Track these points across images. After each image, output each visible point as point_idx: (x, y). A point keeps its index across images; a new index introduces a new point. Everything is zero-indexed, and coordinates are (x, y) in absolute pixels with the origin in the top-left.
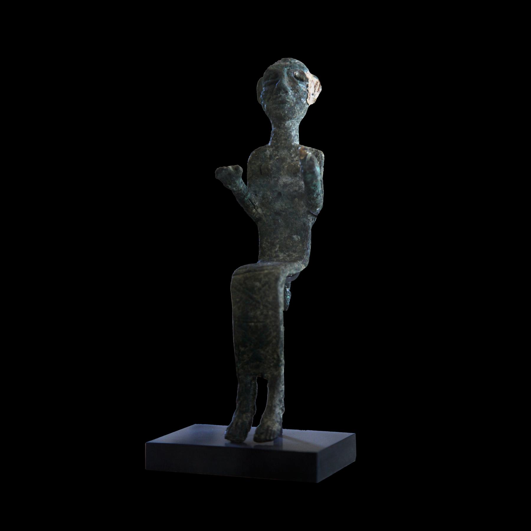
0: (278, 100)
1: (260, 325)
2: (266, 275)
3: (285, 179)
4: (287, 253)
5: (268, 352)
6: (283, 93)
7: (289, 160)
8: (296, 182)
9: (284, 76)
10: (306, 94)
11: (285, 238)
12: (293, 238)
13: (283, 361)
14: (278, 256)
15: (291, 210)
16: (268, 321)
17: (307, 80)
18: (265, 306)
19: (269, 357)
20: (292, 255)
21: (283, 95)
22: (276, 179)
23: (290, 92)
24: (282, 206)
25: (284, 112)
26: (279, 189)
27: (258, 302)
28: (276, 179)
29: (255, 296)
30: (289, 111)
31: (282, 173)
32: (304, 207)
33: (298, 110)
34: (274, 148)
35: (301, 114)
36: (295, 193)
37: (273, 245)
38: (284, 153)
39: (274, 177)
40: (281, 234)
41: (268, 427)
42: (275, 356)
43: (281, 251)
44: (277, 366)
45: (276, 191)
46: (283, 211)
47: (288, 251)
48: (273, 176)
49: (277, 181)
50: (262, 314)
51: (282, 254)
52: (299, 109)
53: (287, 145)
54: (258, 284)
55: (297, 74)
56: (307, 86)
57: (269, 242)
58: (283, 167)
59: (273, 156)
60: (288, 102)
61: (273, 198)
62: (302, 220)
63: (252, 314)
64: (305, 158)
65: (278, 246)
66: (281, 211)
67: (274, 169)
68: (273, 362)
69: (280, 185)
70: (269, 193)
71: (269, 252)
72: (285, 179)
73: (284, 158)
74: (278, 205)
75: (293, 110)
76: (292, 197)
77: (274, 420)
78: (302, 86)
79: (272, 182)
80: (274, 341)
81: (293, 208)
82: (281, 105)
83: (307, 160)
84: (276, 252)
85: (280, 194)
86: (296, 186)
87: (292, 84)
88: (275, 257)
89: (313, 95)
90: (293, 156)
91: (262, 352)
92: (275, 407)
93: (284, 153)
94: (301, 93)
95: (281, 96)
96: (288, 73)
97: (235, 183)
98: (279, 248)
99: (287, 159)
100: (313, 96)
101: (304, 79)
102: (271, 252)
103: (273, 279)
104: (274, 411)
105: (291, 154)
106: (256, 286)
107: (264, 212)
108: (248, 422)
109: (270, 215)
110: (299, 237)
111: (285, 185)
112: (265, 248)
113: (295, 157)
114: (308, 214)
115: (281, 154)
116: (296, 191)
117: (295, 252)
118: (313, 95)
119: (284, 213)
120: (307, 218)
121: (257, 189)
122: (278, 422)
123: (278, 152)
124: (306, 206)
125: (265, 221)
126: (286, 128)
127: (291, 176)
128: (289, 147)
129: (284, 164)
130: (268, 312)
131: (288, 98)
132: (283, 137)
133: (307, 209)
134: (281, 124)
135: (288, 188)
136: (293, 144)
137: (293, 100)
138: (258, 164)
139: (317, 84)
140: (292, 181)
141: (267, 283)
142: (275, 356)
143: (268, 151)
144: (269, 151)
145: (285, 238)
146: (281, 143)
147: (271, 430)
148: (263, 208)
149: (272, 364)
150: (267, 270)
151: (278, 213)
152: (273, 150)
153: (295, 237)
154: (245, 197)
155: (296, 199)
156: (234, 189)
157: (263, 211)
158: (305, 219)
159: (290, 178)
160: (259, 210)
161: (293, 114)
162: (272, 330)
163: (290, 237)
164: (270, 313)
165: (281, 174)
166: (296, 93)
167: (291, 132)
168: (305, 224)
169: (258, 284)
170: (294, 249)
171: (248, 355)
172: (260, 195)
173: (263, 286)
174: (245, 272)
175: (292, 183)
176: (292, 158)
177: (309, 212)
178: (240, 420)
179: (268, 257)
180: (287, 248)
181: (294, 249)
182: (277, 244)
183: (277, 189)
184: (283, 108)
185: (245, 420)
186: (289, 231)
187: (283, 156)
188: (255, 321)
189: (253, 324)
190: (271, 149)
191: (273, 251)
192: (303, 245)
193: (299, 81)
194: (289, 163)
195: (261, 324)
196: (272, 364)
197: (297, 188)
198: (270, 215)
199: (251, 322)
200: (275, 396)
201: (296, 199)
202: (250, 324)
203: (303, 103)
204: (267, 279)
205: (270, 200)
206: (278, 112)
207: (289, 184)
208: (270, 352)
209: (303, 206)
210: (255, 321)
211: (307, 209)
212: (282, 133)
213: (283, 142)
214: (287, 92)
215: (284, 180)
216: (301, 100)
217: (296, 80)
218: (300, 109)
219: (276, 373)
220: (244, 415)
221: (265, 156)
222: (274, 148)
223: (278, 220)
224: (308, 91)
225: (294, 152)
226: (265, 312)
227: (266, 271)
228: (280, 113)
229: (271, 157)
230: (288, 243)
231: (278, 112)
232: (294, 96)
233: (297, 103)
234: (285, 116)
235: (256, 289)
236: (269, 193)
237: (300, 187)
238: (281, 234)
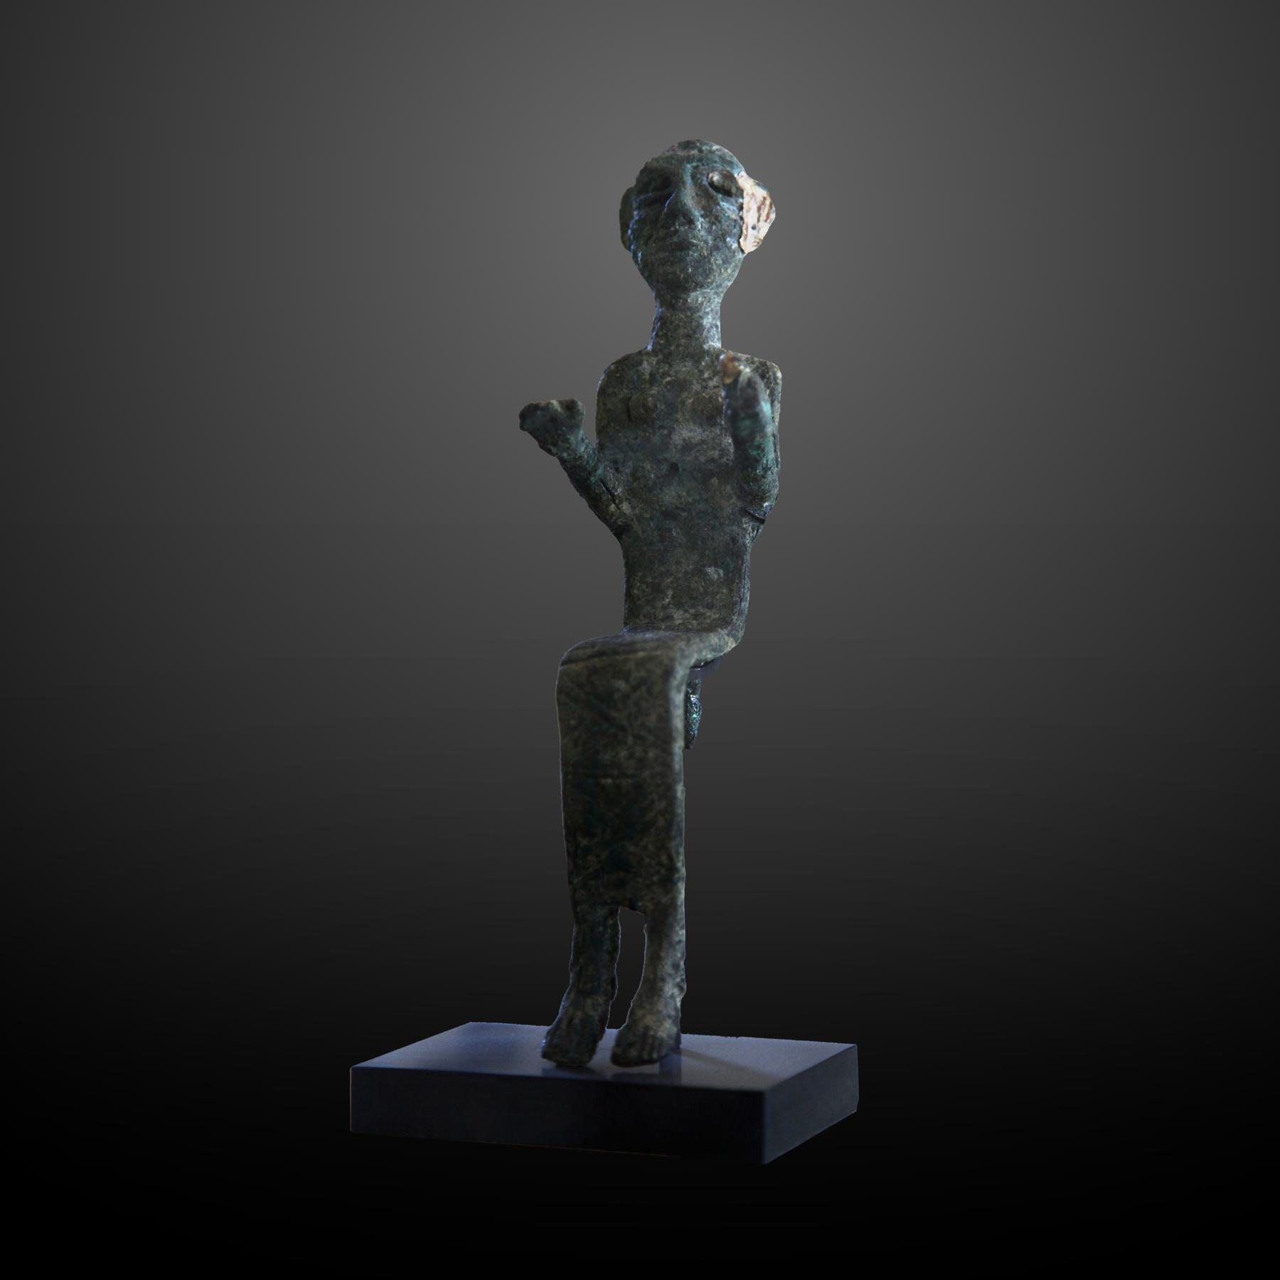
0: (669, 241)
1: (626, 783)
2: (641, 663)
3: (688, 432)
4: (692, 611)
5: (645, 848)
6: (683, 225)
7: (696, 387)
8: (713, 439)
9: (684, 183)
10: (738, 227)
11: (686, 573)
12: (706, 574)
13: (683, 871)
14: (670, 618)
15: (701, 506)
16: (646, 774)
17: (740, 192)
18: (638, 738)
19: (647, 860)
20: (703, 614)
21: (682, 229)
22: (665, 432)
23: (700, 223)
24: (679, 496)
25: (684, 270)
26: (673, 455)
27: (623, 729)
28: (665, 432)
29: (614, 714)
30: (695, 268)
31: (679, 416)
32: (734, 500)
33: (718, 266)
34: (660, 357)
35: (725, 275)
36: (711, 466)
37: (658, 590)
38: (684, 369)
39: (661, 427)
40: (678, 563)
41: (647, 1028)
42: (664, 859)
43: (679, 605)
44: (668, 882)
45: (666, 460)
46: (683, 510)
47: (693, 606)
48: (658, 423)
49: (669, 435)
50: (631, 756)
51: (681, 612)
52: (720, 262)
53: (691, 350)
54: (621, 685)
55: (716, 177)
56: (741, 208)
57: (647, 584)
58: (683, 403)
59: (658, 376)
60: (693, 245)
61: (657, 477)
62: (727, 529)
63: (607, 757)
64: (736, 381)
65: (670, 593)
66: (677, 508)
67: (661, 406)
68: (658, 872)
69: (676, 446)
70: (648, 466)
71: (648, 608)
72: (688, 432)
73: (685, 381)
74: (670, 495)
75: (707, 266)
76: (704, 475)
77: (660, 1012)
78: (728, 207)
79: (656, 439)
80: (661, 822)
81: (706, 500)
82: (678, 253)
83: (739, 386)
84: (665, 607)
85: (674, 467)
86: (714, 448)
87: (704, 202)
88: (662, 620)
89: (754, 228)
90: (706, 375)
91: (632, 848)
92: (663, 980)
93: (684, 369)
94: (725, 225)
95: (677, 231)
96: (693, 177)
97: (567, 441)
98: (673, 597)
99: (691, 384)
100: (755, 232)
101: (734, 190)
102: (654, 607)
103: (659, 672)
104: (661, 990)
105: (701, 372)
106: (618, 690)
107: (637, 511)
108: (597, 1018)
109: (651, 518)
110: (721, 572)
111: (688, 446)
112: (639, 599)
113: (710, 378)
114: (743, 516)
115: (677, 372)
116: (713, 460)
117: (710, 606)
118: (754, 228)
119: (684, 514)
120: (740, 527)
121: (620, 456)
122: (669, 1017)
123: (671, 366)
124: (739, 497)
125: (640, 532)
126: (689, 308)
127: (701, 425)
128: (698, 354)
129: (685, 394)
130: (646, 752)
131: (694, 237)
132: (681, 331)
133: (739, 504)
134: (677, 298)
135: (693, 454)
136: (706, 347)
137: (706, 242)
138: (621, 396)
139: (763, 203)
140: (704, 435)
141: (643, 682)
143: (645, 365)
144: (649, 363)
145: (686, 573)
146: (678, 346)
147: (654, 1037)
148: (634, 501)
149: (655, 879)
150: (643, 650)
151: (669, 514)
152: (658, 362)
153: (711, 570)
154: (590, 474)
155: (715, 481)
157: (633, 508)
158: (735, 528)
159: (700, 430)
160: (625, 507)
161: (707, 276)
162: (655, 796)
163: (700, 572)
164: (651, 754)
165: (677, 420)
166: (713, 223)
167: (701, 317)
168: (734, 540)
169: (621, 685)
170: (708, 599)
171: (598, 856)
172: (628, 471)
173: (635, 689)
174: (591, 657)
175: (703, 442)
176: (705, 380)
177: (745, 512)
178: (579, 1013)
179: (647, 621)
180: (691, 598)
181: (708, 599)
182: (669, 587)
183: (667, 455)
184: (682, 260)
185: (591, 1013)
186: (696, 557)
187: (681, 376)
188: (616, 773)
189: (609, 781)
190: (654, 360)
191: (659, 605)
192: (731, 591)
193: (720, 196)
194: (697, 393)
195: (630, 781)
196: (655, 879)
197: (716, 454)
198: (651, 518)
199: (606, 776)
200: (663, 954)
201: (715, 481)
202: (603, 781)
203: (729, 248)
204: (643, 673)
205: (651, 483)
206: (669, 269)
207: (697, 445)
208: (651, 847)
209: (730, 497)
210: (616, 773)
211: (739, 504)
212: (681, 320)
213: (683, 341)
214: (691, 222)
215: (685, 434)
216: (725, 240)
217: (714, 193)
218: (724, 262)
219: (664, 900)
220: (589, 1002)
221: (639, 377)
222: (660, 357)
223: (669, 530)
224: (742, 218)
225: (708, 366)
226: (639, 752)
227: (641, 654)
228: (675, 273)
229: (653, 380)
230: (693, 585)
231: (669, 269)
232: (709, 231)
233: (716, 248)
234: (686, 280)
235: (616, 696)
236: (648, 466)
237: (723, 452)
238: (678, 563)
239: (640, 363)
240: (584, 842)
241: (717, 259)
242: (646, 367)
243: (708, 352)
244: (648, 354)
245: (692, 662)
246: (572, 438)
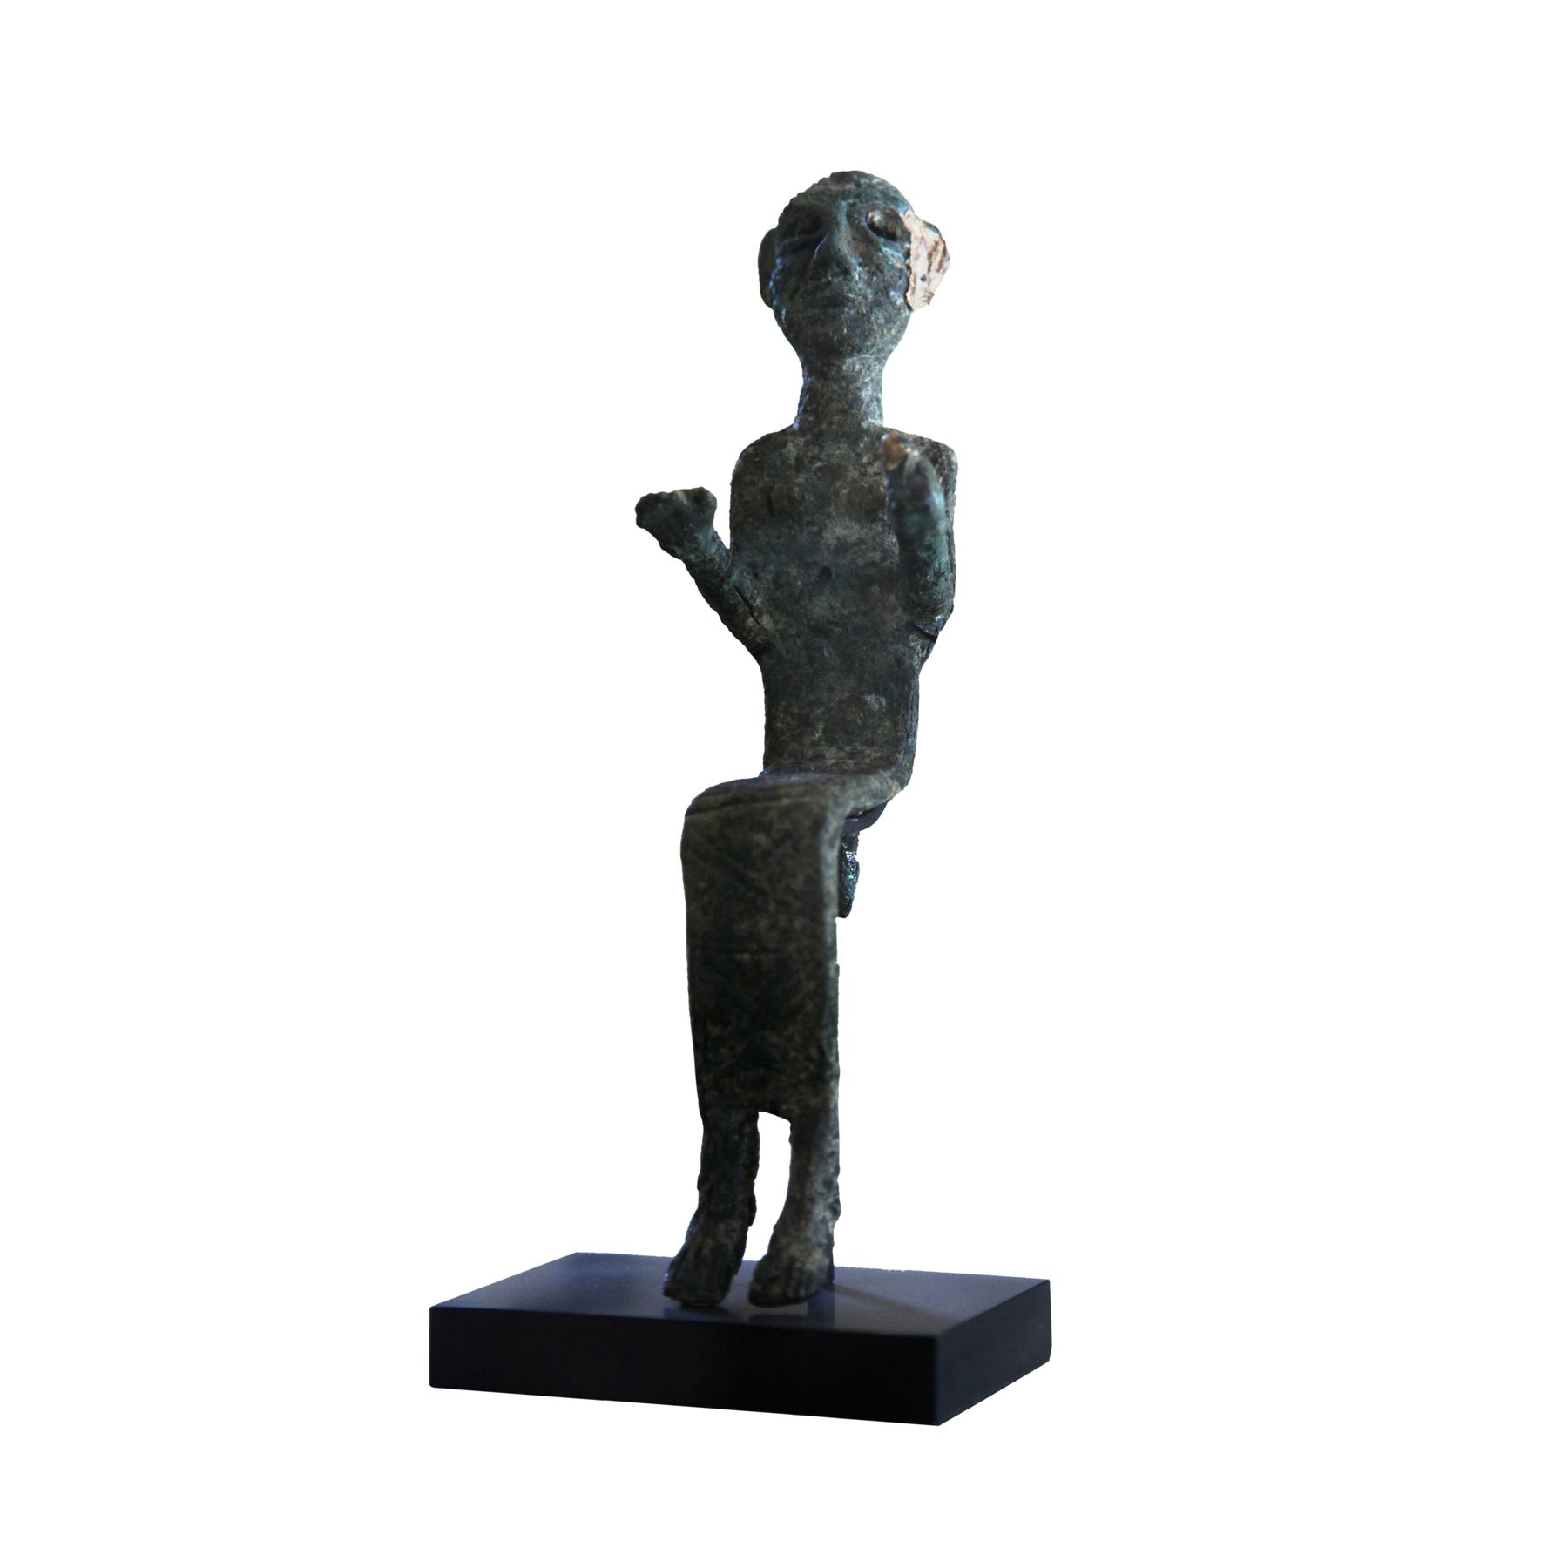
0: (820, 295)
1: (767, 959)
2: (786, 812)
3: (843, 529)
4: (848, 749)
5: (791, 1039)
6: (837, 275)
7: (853, 474)
8: (874, 538)
9: (838, 224)
11: (840, 702)
12: (865, 703)
14: (820, 756)
15: (858, 620)
16: (792, 948)
18: (782, 904)
19: (793, 1054)
20: (861, 752)
21: (835, 280)
22: (815, 529)
23: (858, 273)
24: (832, 608)
25: (838, 330)
26: (824, 557)
27: (763, 893)
28: (815, 529)
29: (753, 875)
30: (852, 329)
31: (832, 509)
32: (899, 612)
33: (879, 325)
34: (809, 437)
35: (888, 337)
36: (871, 571)
37: (806, 723)
39: (810, 524)
40: (831, 690)
41: (793, 1260)
42: (813, 1052)
43: (831, 741)
45: (815, 563)
46: (837, 624)
47: (850, 742)
48: (806, 518)
49: (819, 533)
50: (773, 926)
51: (834, 750)
52: (882, 321)
53: (846, 429)
54: (761, 839)
55: (877, 217)
56: (908, 255)
57: (793, 716)
58: (837, 493)
59: (806, 461)
60: (849, 300)
61: (805, 585)
62: (891, 649)
63: (743, 927)
64: (902, 466)
65: (821, 726)
66: (829, 622)
67: (810, 498)
68: (806, 1068)
69: (828, 547)
70: (793, 571)
71: (794, 745)
72: (843, 529)
73: (839, 466)
74: (821, 607)
75: (866, 326)
76: (862, 582)
77: (808, 1240)
78: (891, 253)
79: (803, 538)
80: (810, 1007)
81: (865, 613)
82: (831, 311)
83: (906, 473)
84: (814, 744)
85: (826, 573)
86: (874, 549)
87: (862, 248)
88: (811, 760)
89: (923, 279)
90: (865, 460)
91: (774, 1039)
92: (812, 1200)
93: (838, 451)
94: (888, 275)
95: (829, 283)
96: (849, 217)
97: (695, 540)
98: (825, 731)
99: (847, 470)
100: (925, 284)
101: (899, 233)
102: (801, 744)
103: (807, 823)
104: (810, 1213)
105: (859, 456)
106: (757, 845)
107: (780, 627)
109: (798, 635)
110: (883, 701)
111: (842, 547)
112: (783, 734)
113: (870, 464)
114: (910, 632)
115: (829, 456)
116: (873, 564)
117: (870, 743)
118: (923, 279)
119: (838, 630)
120: (907, 645)
121: (759, 559)
123: (822, 448)
124: (905, 609)
125: (784, 652)
126: (844, 378)
127: (859, 521)
129: (839, 483)
130: (791, 921)
131: (851, 290)
132: (835, 406)
133: (906, 618)
134: (830, 365)
135: (849, 556)
136: (865, 425)
137: (865, 297)
138: (761, 485)
140: (863, 533)
141: (787, 835)
143: (790, 447)
144: (795, 445)
145: (840, 702)
146: (830, 424)
147: (801, 1271)
148: (776, 613)
149: (803, 1076)
150: (788, 796)
151: (820, 630)
152: (807, 444)
153: (870, 698)
154: (722, 580)
155: (875, 589)
157: (776, 622)
158: (900, 647)
159: (857, 527)
160: (766, 621)
161: (866, 338)
162: (802, 975)
163: (857, 700)
164: (798, 924)
165: (829, 515)
166: (874, 274)
167: (859, 389)
168: (899, 662)
169: (761, 839)
170: (868, 734)
171: (732, 1049)
172: (769, 577)
173: (778, 843)
174: (724, 804)
175: (861, 541)
176: (863, 465)
178: (710, 1242)
179: (792, 760)
180: (847, 732)
181: (868, 734)
182: (819, 719)
183: (817, 558)
184: (835, 318)
185: (724, 1241)
186: (852, 683)
187: (834, 461)
188: (754, 946)
189: (746, 956)
190: (801, 441)
191: (807, 741)
192: (895, 723)
193: (882, 240)
194: (854, 481)
195: (771, 956)
196: (803, 1076)
197: (877, 556)
198: (798, 635)
199: (742, 951)
200: (812, 1169)
201: (875, 589)
202: (739, 957)
203: (893, 304)
204: (788, 825)
205: (797, 592)
206: (819, 329)
207: (853, 545)
208: (797, 1038)
209: (894, 609)
210: (754, 946)
211: (906, 618)
212: (834, 392)
213: (836, 418)
214: (846, 272)
215: (840, 531)
216: (888, 295)
217: (875, 237)
218: (887, 322)
219: (814, 1102)
220: (722, 1227)
221: (783, 462)
222: (809, 437)
223: (820, 649)
224: (909, 267)
225: (867, 449)
226: (782, 921)
227: (785, 801)
228: (826, 334)
230: (849, 717)
231: (819, 329)
232: (869, 283)
233: (877, 304)
234: (841, 343)
235: (755, 853)
236: (793, 571)
237: (886, 553)
238: (831, 690)
239: (784, 445)
241: (879, 317)
243: (867, 432)
245: (848, 810)
246: (701, 537)
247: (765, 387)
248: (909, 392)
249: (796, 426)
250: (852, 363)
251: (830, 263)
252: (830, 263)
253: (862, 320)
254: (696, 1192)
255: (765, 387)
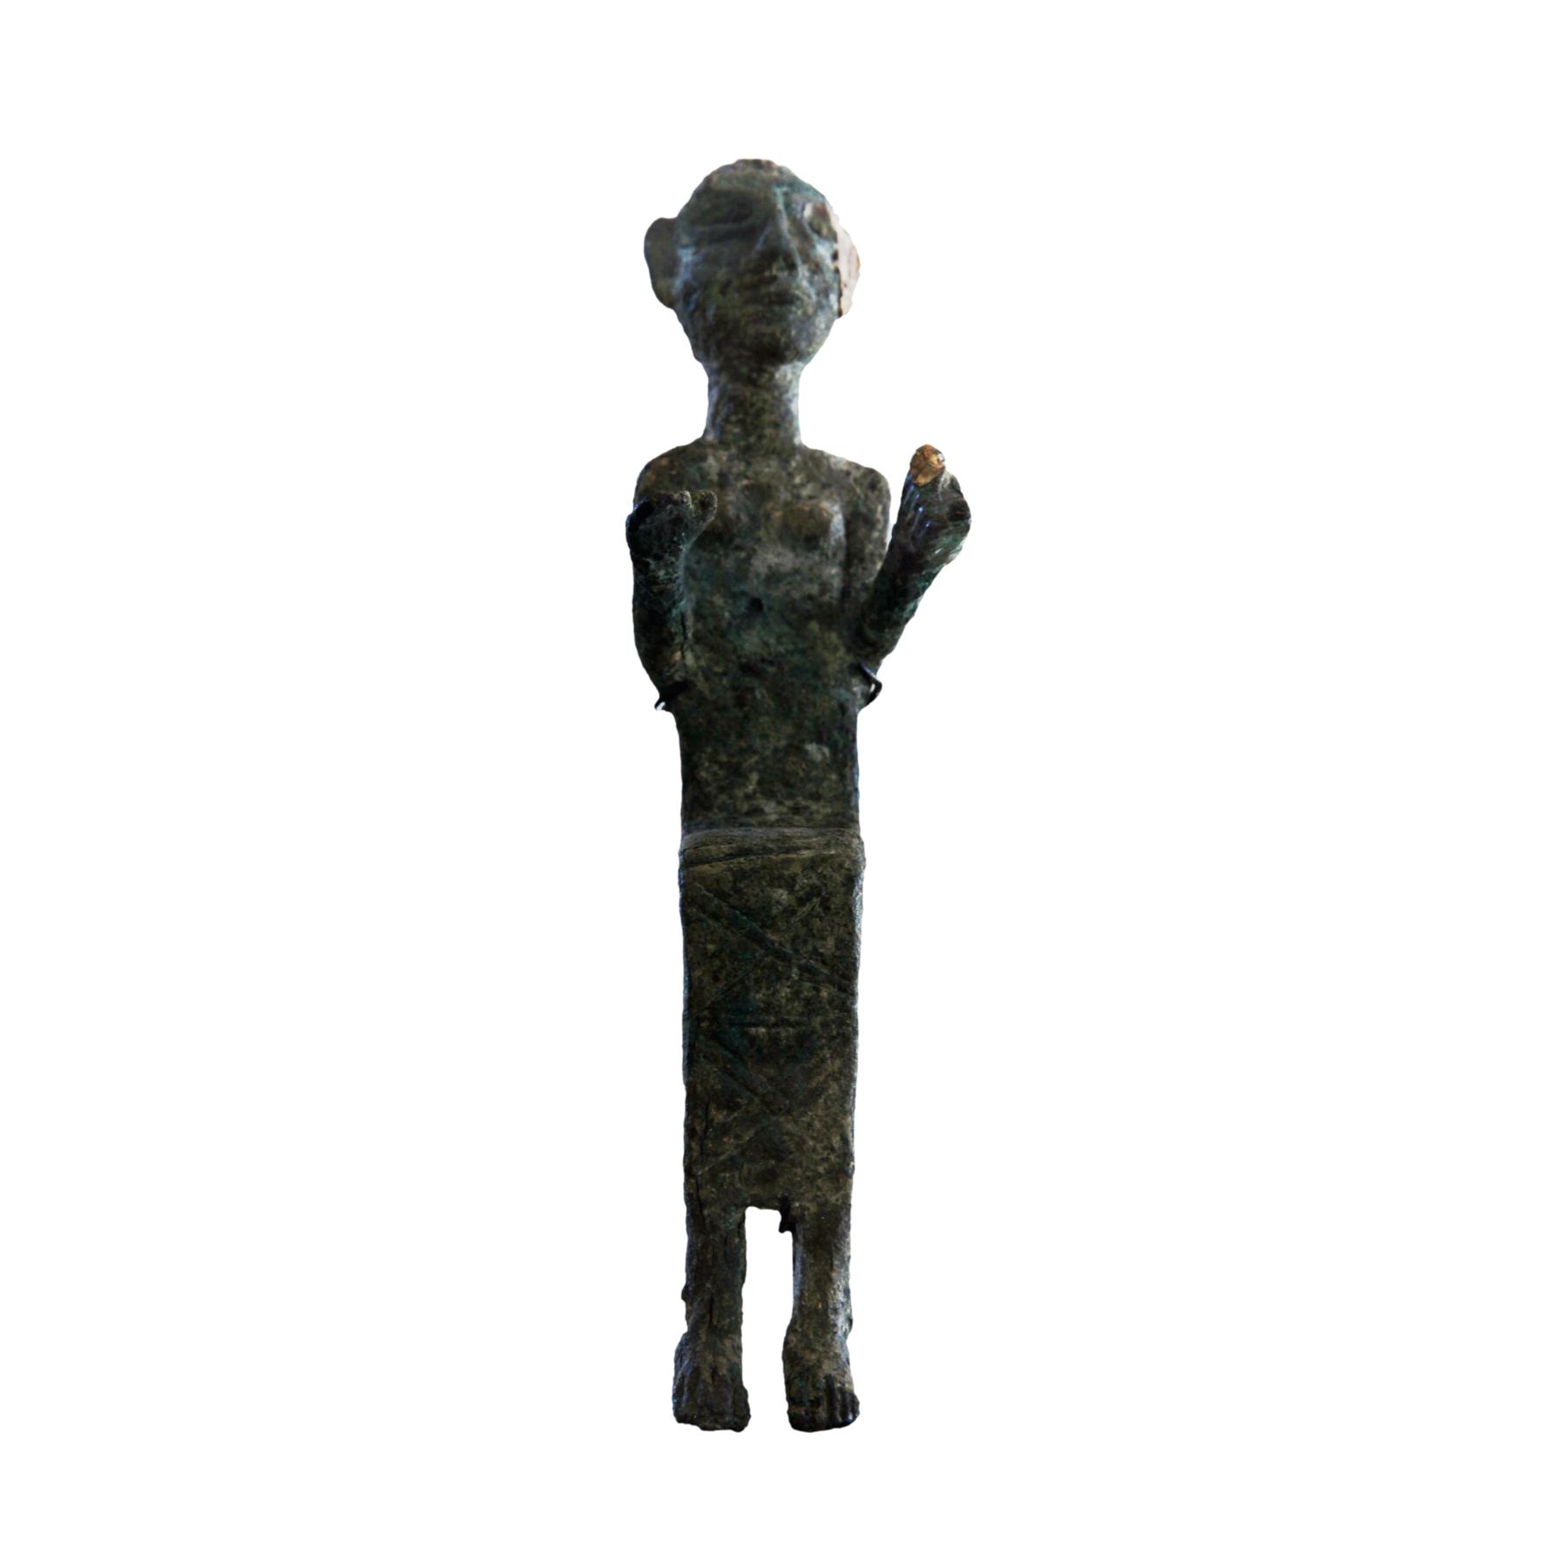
0: (763, 290)
3: (773, 557)
4: (789, 803)
5: (810, 1125)
6: (781, 269)
7: (784, 495)
8: (811, 569)
11: (776, 750)
12: (806, 752)
14: (756, 811)
15: (796, 659)
16: (817, 1021)
19: (811, 1143)
20: (807, 808)
22: (743, 555)
24: (766, 644)
25: (785, 331)
26: (754, 587)
27: (784, 957)
28: (743, 555)
29: (771, 936)
31: (762, 533)
32: (842, 652)
34: (733, 450)
36: (808, 606)
37: (737, 773)
38: (768, 469)
39: (739, 548)
40: (764, 736)
41: (829, 1378)
45: (743, 593)
46: (771, 663)
47: (791, 796)
48: (738, 541)
49: (749, 558)
50: (797, 994)
53: (778, 444)
56: (835, 256)
57: (721, 766)
58: (768, 516)
59: (731, 478)
61: (734, 617)
62: (834, 692)
63: (759, 996)
64: (936, 481)
65: (755, 777)
66: (763, 660)
67: (744, 518)
69: (758, 575)
70: (718, 600)
71: (723, 798)
72: (773, 557)
73: (769, 487)
74: (751, 642)
76: (799, 615)
79: (729, 564)
81: (803, 652)
82: (777, 308)
83: (940, 489)
84: (748, 797)
85: (756, 605)
86: (811, 581)
88: (748, 814)
90: (797, 480)
91: (789, 1127)
93: (768, 469)
95: (774, 279)
98: (760, 783)
99: (777, 489)
101: (825, 231)
103: (839, 878)
104: (835, 1325)
105: (791, 475)
107: (703, 663)
109: (725, 674)
110: (826, 750)
111: (774, 577)
112: (708, 784)
113: (803, 485)
114: (852, 675)
115: (757, 474)
116: (810, 597)
117: (816, 797)
119: (772, 670)
120: (849, 689)
123: (748, 464)
124: (849, 650)
125: (707, 692)
127: (794, 549)
129: (770, 505)
130: (818, 990)
132: (767, 418)
133: (850, 659)
134: (761, 371)
135: (783, 588)
140: (798, 563)
141: (814, 891)
142: (836, 1141)
143: (711, 461)
144: (718, 459)
145: (776, 750)
146: (761, 437)
148: (697, 648)
149: (821, 1169)
150: (807, 848)
151: (748, 668)
152: (731, 459)
153: (811, 748)
155: (814, 626)
156: (662, 573)
157: (697, 658)
158: (842, 691)
159: (791, 555)
163: (796, 748)
164: (824, 994)
165: (759, 540)
169: (782, 895)
171: (737, 1137)
174: (731, 856)
175: (796, 571)
176: (795, 486)
179: (724, 814)
180: (787, 784)
181: (811, 787)
182: (751, 770)
184: (782, 318)
186: (789, 729)
187: (764, 480)
189: (763, 1030)
190: (724, 455)
191: (739, 793)
194: (787, 504)
196: (821, 1169)
197: (814, 589)
198: (725, 674)
199: (756, 1025)
200: (834, 1275)
201: (814, 626)
202: (753, 1030)
204: (814, 880)
205: (724, 624)
206: (764, 329)
207: (786, 575)
208: (817, 1124)
209: (836, 649)
210: (773, 1019)
211: (850, 659)
212: (765, 401)
215: (772, 559)
222: (733, 450)
223: (752, 690)
225: (799, 469)
226: (807, 990)
227: (806, 854)
228: (773, 335)
229: (723, 482)
231: (764, 329)
232: (811, 282)
234: (787, 347)
236: (718, 600)
237: (825, 587)
239: (703, 458)
240: (719, 1117)
241: (821, 321)
242: (712, 464)
244: (712, 446)
247: (672, 397)
248: (849, 406)
249: (710, 438)
250: (785, 372)
251: (742, 265)
252: (742, 265)
253: (808, 319)
254: (682, 1306)
255: (672, 397)
